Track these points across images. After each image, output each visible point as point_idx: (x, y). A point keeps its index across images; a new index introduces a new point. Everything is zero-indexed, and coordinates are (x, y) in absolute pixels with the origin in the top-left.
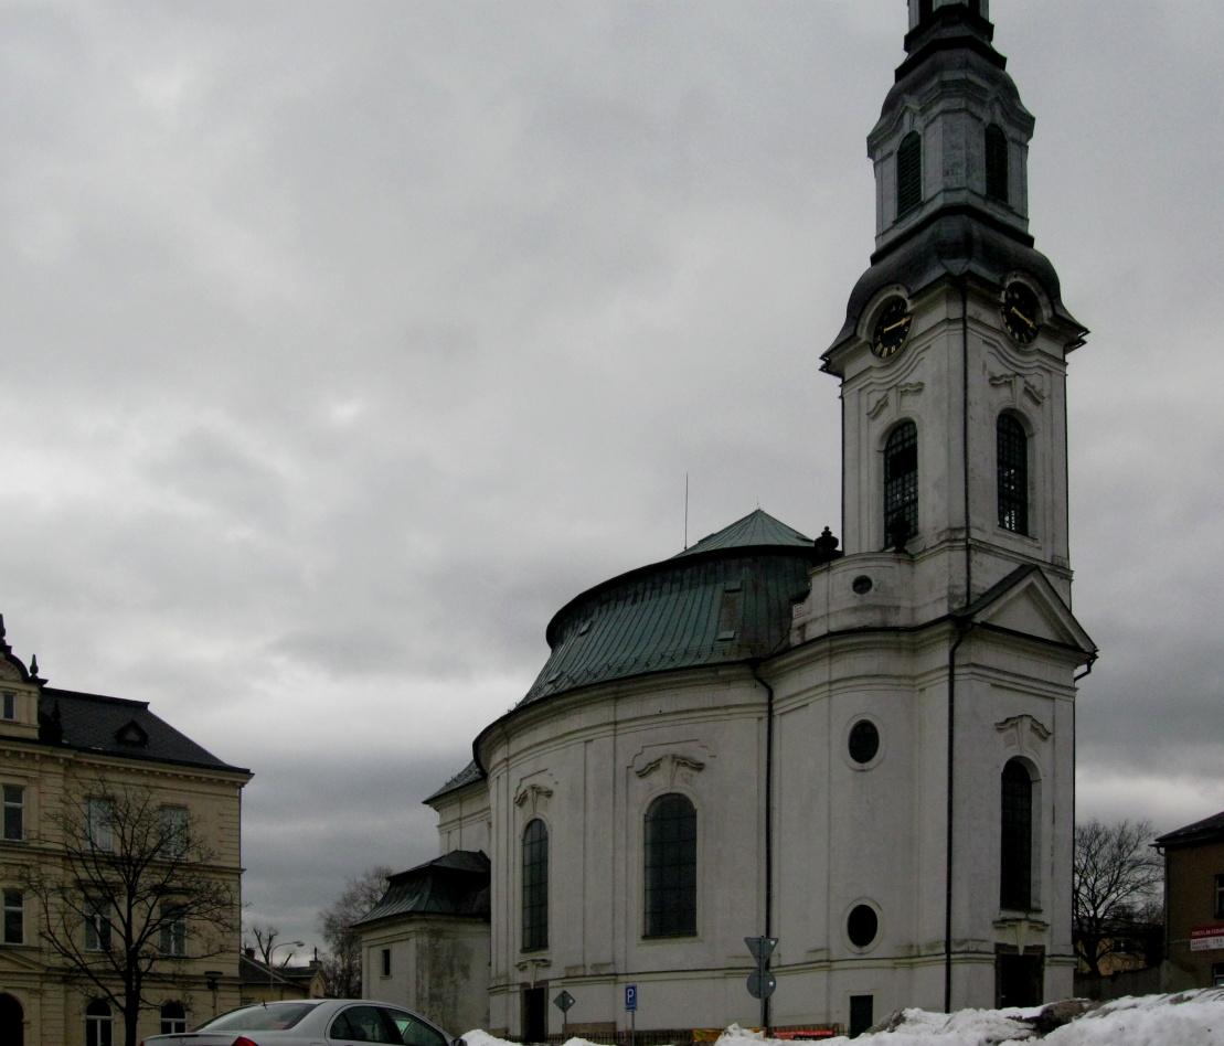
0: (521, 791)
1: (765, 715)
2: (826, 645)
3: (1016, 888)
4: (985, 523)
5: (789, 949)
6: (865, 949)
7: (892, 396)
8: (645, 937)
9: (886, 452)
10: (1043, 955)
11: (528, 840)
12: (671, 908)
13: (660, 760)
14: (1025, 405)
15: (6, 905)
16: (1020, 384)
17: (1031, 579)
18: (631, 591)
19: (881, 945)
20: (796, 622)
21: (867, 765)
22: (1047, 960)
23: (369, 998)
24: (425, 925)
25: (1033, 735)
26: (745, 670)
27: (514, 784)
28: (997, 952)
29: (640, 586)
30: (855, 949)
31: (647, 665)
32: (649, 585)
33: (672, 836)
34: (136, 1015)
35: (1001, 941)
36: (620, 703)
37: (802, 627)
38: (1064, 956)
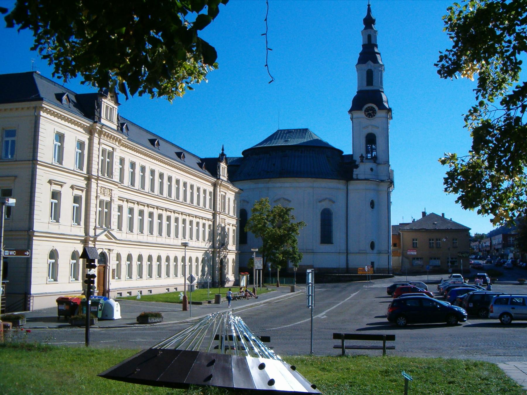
12: (326, 237)
15: (74, 203)
19: (375, 251)
33: (326, 219)
38: (96, 219)
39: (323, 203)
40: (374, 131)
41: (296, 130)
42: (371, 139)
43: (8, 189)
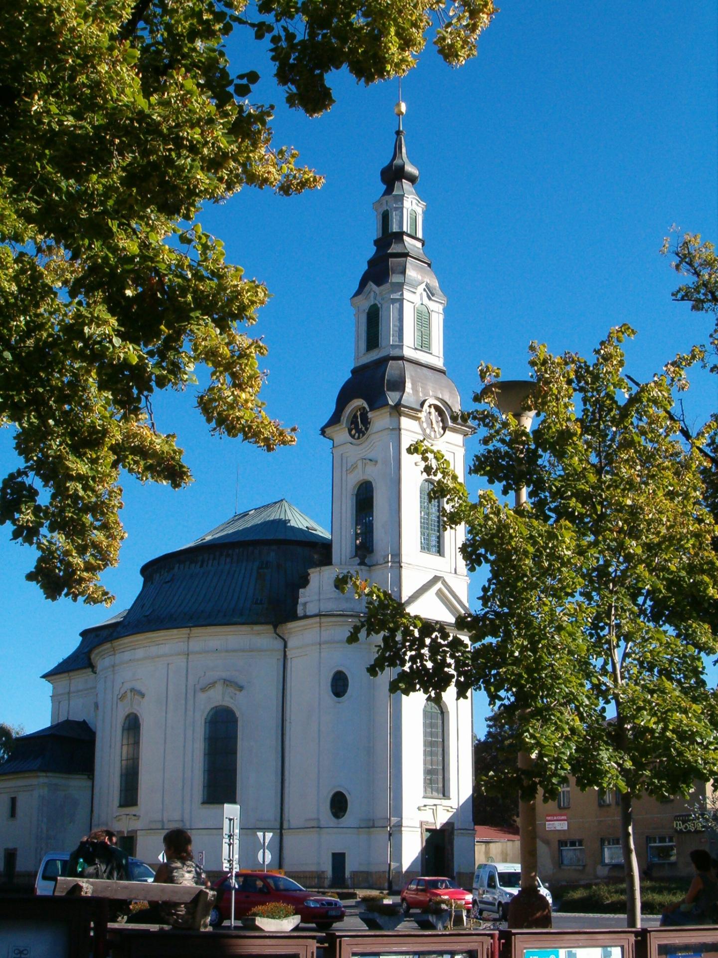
0: (122, 691)
5: (294, 816)
8: (203, 803)
13: (215, 682)
17: (439, 585)
18: (200, 558)
19: (349, 818)
22: (456, 832)
23: (642, 920)
24: (46, 780)
37: (305, 604)
39: (211, 693)
40: (371, 473)
41: (296, 541)
42: (364, 500)
43: (5, 857)
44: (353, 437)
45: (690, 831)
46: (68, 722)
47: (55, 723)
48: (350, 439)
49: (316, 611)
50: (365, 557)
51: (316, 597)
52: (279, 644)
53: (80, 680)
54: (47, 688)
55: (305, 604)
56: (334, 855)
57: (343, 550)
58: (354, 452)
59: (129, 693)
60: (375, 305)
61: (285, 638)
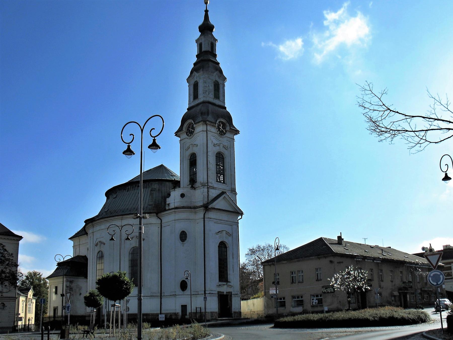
1: (160, 227)
2: (174, 210)
3: (223, 276)
4: (213, 181)
5: (167, 291)
6: (185, 292)
7: (191, 146)
9: (190, 159)
10: (231, 294)
11: (98, 256)
14: (223, 150)
16: (222, 145)
20: (167, 203)
21: (184, 243)
22: (233, 296)
25: (227, 235)
26: (155, 214)
27: (95, 240)
28: (218, 294)
29: (129, 187)
30: (183, 292)
31: (130, 211)
32: (132, 187)
34: (400, 319)
35: (220, 290)
36: (123, 220)
37: (169, 204)
44: (188, 135)
45: (328, 292)
46: (78, 256)
47: (75, 256)
48: (187, 137)
49: (173, 207)
50: (193, 184)
51: (173, 201)
52: (159, 221)
53: (83, 239)
54: (71, 243)
55: (169, 204)
56: (182, 306)
57: (185, 182)
58: (188, 141)
59: (99, 243)
60: (197, 81)
61: (161, 218)
